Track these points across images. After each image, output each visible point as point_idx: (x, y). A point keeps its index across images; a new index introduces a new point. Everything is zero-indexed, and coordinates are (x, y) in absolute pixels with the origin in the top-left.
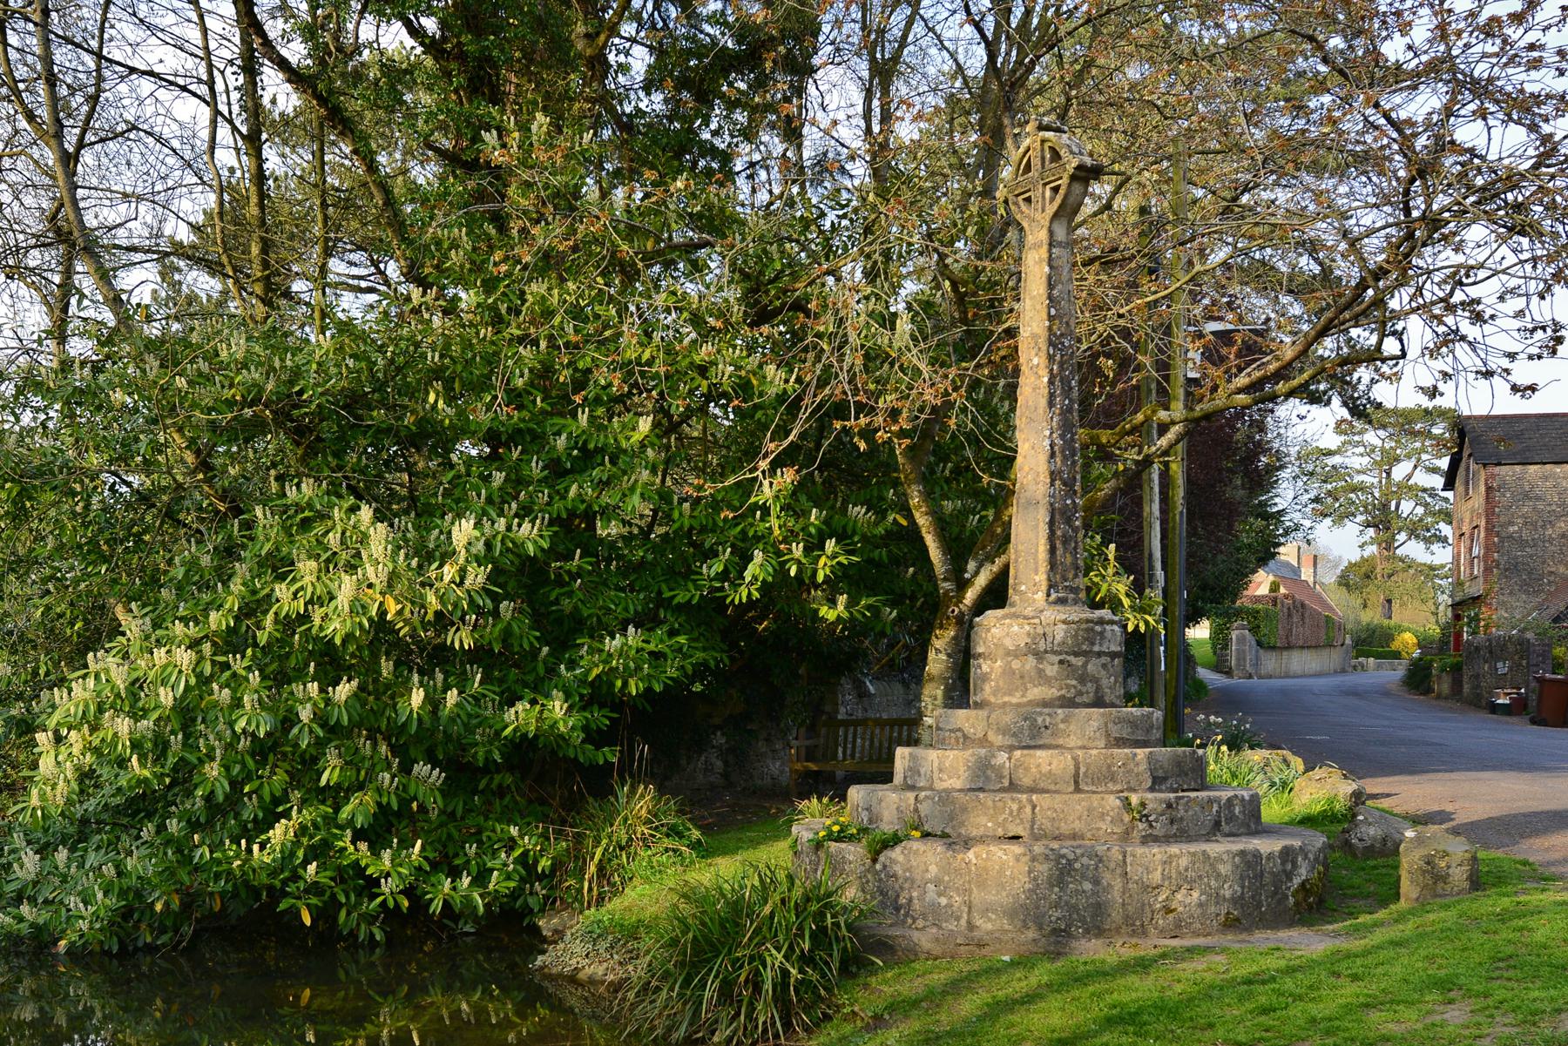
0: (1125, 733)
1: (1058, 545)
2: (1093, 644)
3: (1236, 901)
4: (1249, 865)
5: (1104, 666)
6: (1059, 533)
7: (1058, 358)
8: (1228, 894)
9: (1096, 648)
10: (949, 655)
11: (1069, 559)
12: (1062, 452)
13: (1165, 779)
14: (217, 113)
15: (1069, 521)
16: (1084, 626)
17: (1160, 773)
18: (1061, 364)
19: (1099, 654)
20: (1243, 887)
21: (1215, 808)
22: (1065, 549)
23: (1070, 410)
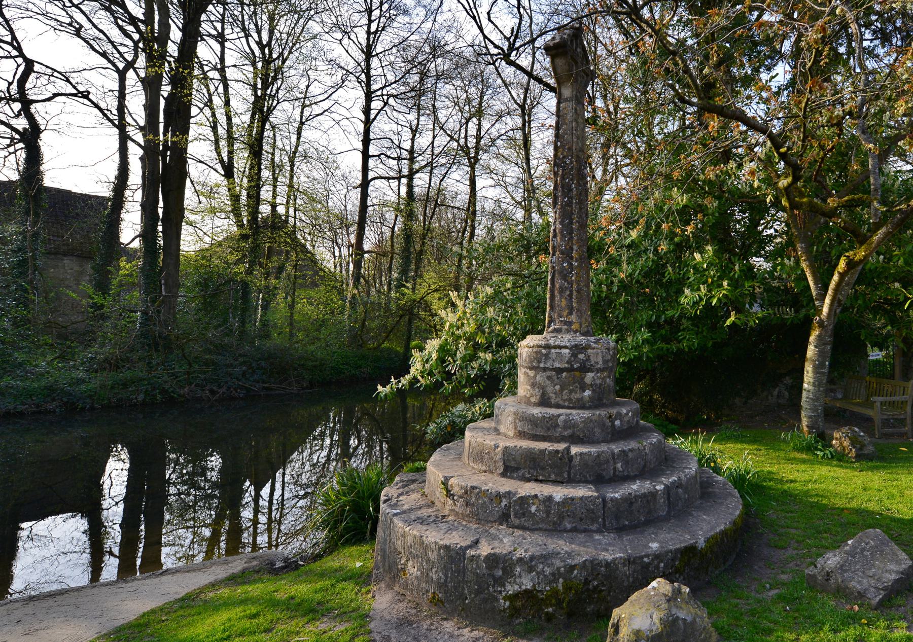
0: (527, 428)
1: (556, 293)
2: (539, 362)
3: (441, 585)
4: (452, 560)
5: (549, 378)
6: (557, 286)
7: (560, 173)
8: (435, 577)
9: (542, 365)
10: (815, 347)
11: (564, 303)
12: (561, 232)
13: (517, 469)
14: (212, 22)
15: (564, 277)
16: (535, 349)
17: (513, 464)
18: (563, 178)
19: (545, 370)
20: (446, 576)
21: (504, 502)
22: (561, 297)
23: (569, 204)
